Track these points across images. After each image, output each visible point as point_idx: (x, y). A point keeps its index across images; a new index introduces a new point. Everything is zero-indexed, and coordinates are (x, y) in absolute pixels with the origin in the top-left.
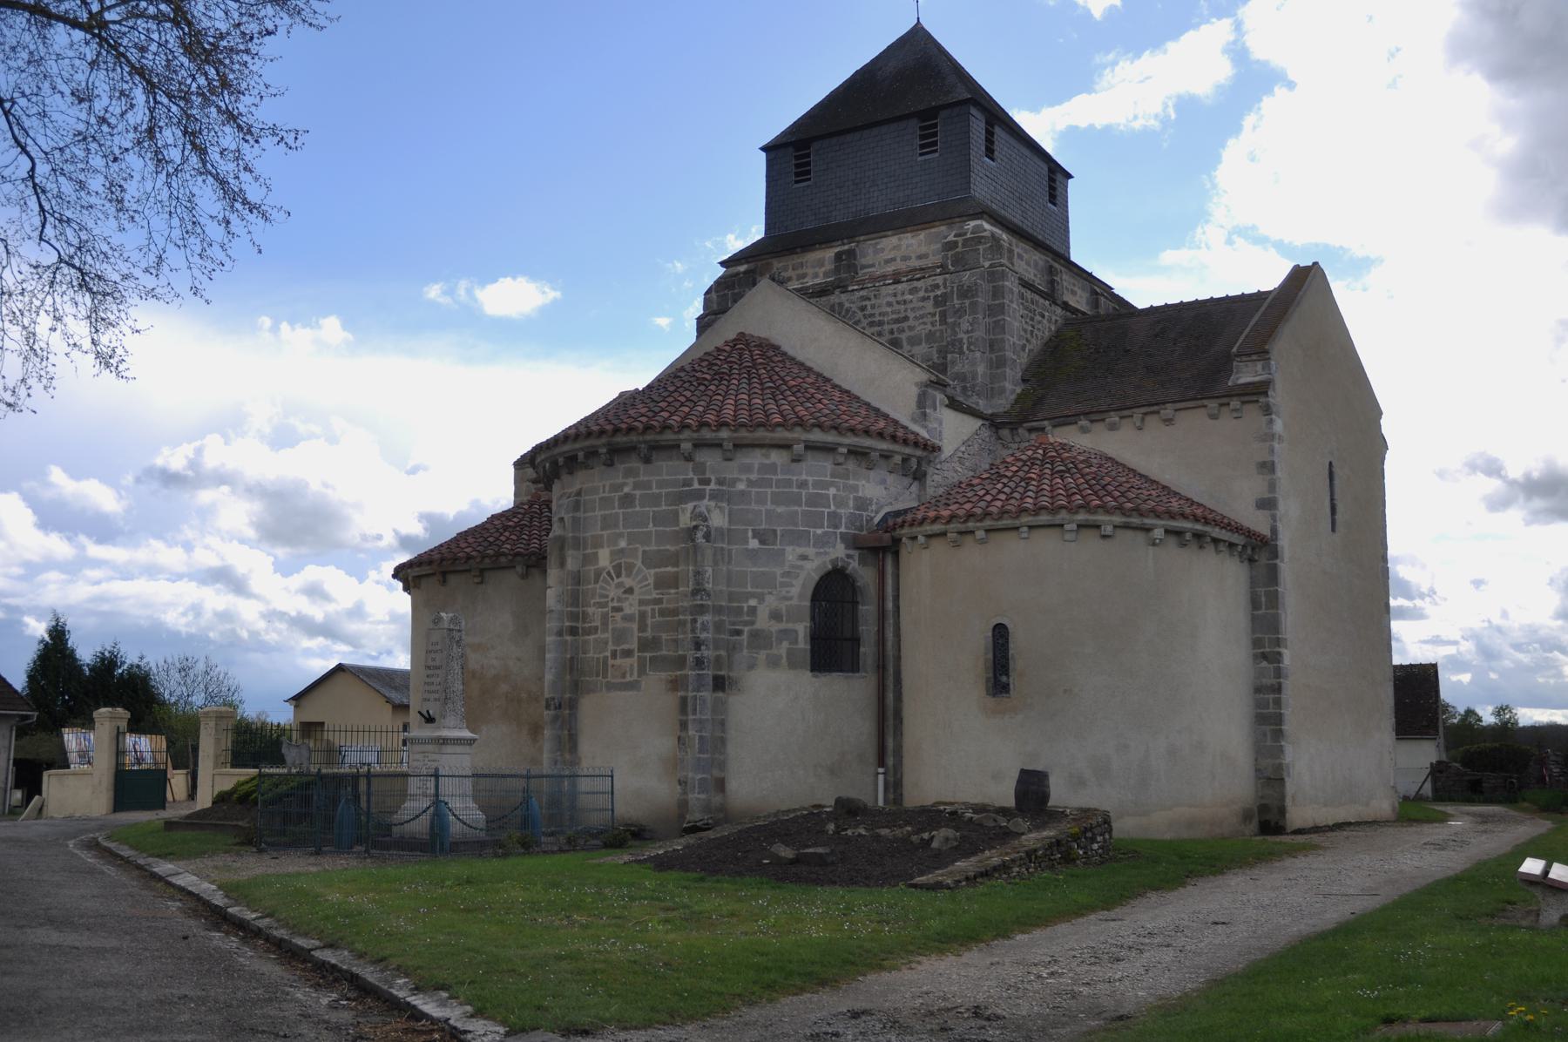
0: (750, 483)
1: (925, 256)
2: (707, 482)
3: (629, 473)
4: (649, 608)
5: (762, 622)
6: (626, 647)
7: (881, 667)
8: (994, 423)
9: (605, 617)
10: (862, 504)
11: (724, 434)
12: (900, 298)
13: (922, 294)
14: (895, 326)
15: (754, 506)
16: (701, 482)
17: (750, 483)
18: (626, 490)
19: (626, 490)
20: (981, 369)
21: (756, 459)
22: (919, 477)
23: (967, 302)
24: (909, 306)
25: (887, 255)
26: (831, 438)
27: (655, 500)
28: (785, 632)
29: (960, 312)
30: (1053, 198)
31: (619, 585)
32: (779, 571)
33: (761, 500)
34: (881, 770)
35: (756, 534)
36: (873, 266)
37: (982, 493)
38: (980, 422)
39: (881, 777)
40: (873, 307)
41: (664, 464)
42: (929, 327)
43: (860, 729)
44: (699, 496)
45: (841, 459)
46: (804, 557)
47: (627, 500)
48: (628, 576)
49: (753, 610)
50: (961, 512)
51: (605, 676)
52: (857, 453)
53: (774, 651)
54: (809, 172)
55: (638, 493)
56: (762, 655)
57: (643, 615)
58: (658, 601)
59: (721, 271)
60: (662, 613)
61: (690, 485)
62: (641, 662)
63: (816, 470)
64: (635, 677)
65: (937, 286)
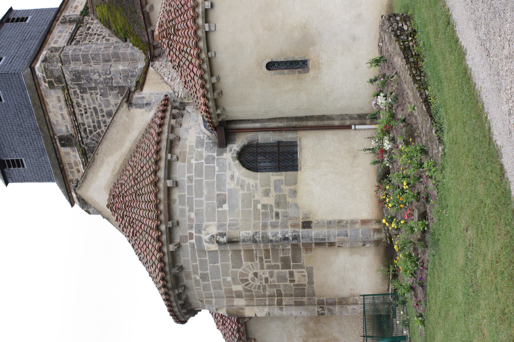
0: (191, 210)
1: (59, 98)
2: (191, 235)
3: (188, 276)
4: (265, 264)
5: (270, 201)
6: (288, 275)
7: (295, 129)
8: (152, 54)
9: (271, 286)
10: (200, 143)
11: (163, 228)
12: (83, 112)
13: (80, 101)
14: (100, 114)
15: (204, 207)
16: (191, 238)
17: (191, 210)
18: (198, 278)
19: (198, 278)
20: (121, 67)
21: (177, 207)
22: (183, 106)
23: (82, 76)
24: (87, 107)
25: (60, 118)
26: (162, 164)
27: (203, 263)
28: (276, 188)
29: (89, 80)
30: (24, 20)
31: (253, 280)
32: (241, 192)
33: (200, 204)
34: (353, 127)
35: (220, 205)
36: (66, 126)
37: (190, 78)
38: (151, 69)
39: (357, 127)
40: (89, 126)
41: (182, 258)
42: (98, 96)
43: (329, 138)
44: (199, 240)
45: (175, 157)
46: (232, 177)
47: (204, 277)
48: (247, 276)
49: (264, 206)
50: (202, 91)
51: (305, 285)
52: (171, 145)
53: (287, 193)
54: (18, 160)
55: (200, 272)
56: (289, 200)
57: (269, 267)
58: (261, 259)
59: (77, 206)
60: (267, 257)
61: (193, 244)
62: (295, 267)
63: (181, 172)
64: (304, 270)
65: (75, 92)
